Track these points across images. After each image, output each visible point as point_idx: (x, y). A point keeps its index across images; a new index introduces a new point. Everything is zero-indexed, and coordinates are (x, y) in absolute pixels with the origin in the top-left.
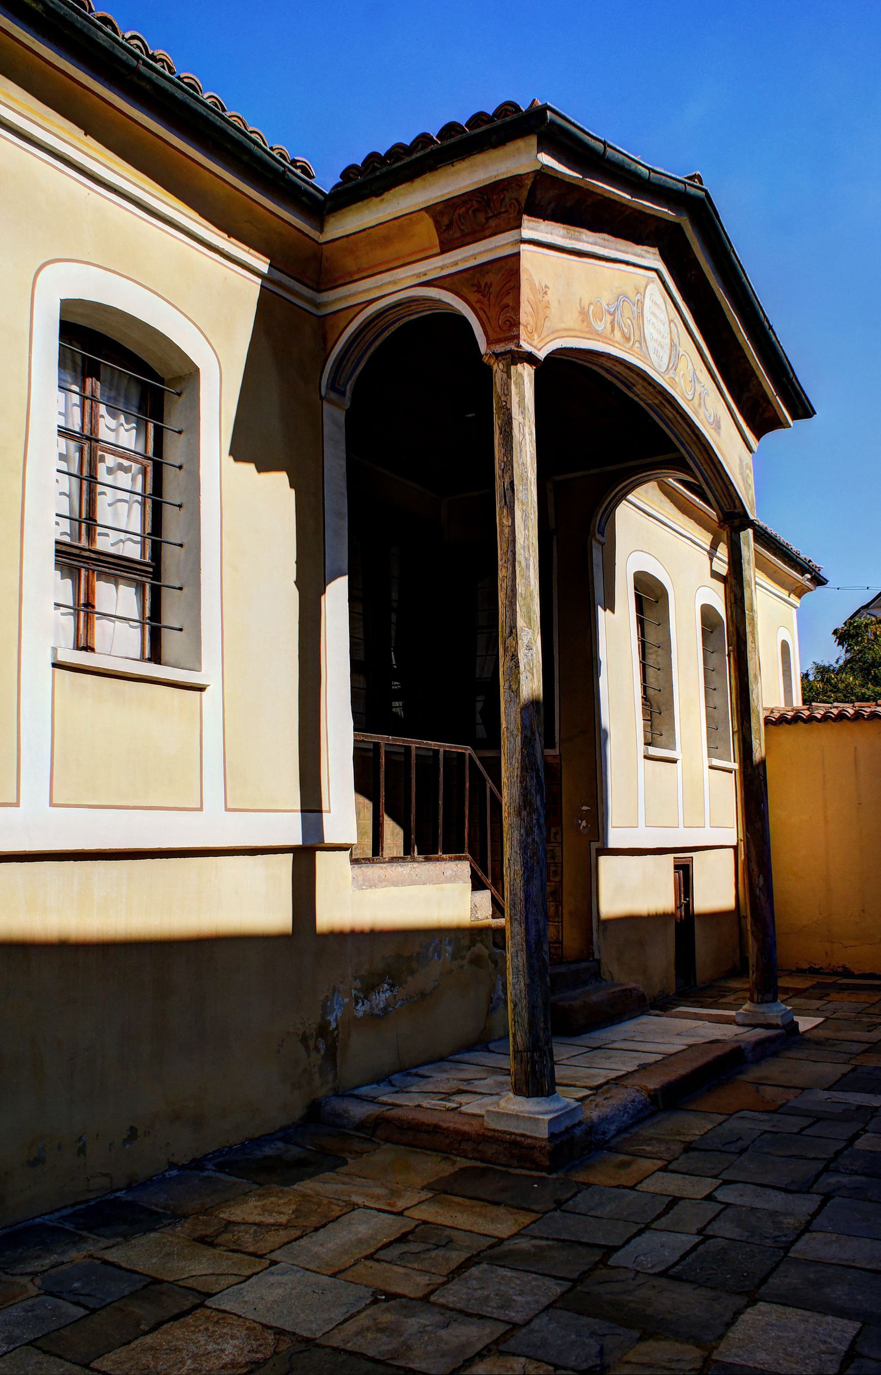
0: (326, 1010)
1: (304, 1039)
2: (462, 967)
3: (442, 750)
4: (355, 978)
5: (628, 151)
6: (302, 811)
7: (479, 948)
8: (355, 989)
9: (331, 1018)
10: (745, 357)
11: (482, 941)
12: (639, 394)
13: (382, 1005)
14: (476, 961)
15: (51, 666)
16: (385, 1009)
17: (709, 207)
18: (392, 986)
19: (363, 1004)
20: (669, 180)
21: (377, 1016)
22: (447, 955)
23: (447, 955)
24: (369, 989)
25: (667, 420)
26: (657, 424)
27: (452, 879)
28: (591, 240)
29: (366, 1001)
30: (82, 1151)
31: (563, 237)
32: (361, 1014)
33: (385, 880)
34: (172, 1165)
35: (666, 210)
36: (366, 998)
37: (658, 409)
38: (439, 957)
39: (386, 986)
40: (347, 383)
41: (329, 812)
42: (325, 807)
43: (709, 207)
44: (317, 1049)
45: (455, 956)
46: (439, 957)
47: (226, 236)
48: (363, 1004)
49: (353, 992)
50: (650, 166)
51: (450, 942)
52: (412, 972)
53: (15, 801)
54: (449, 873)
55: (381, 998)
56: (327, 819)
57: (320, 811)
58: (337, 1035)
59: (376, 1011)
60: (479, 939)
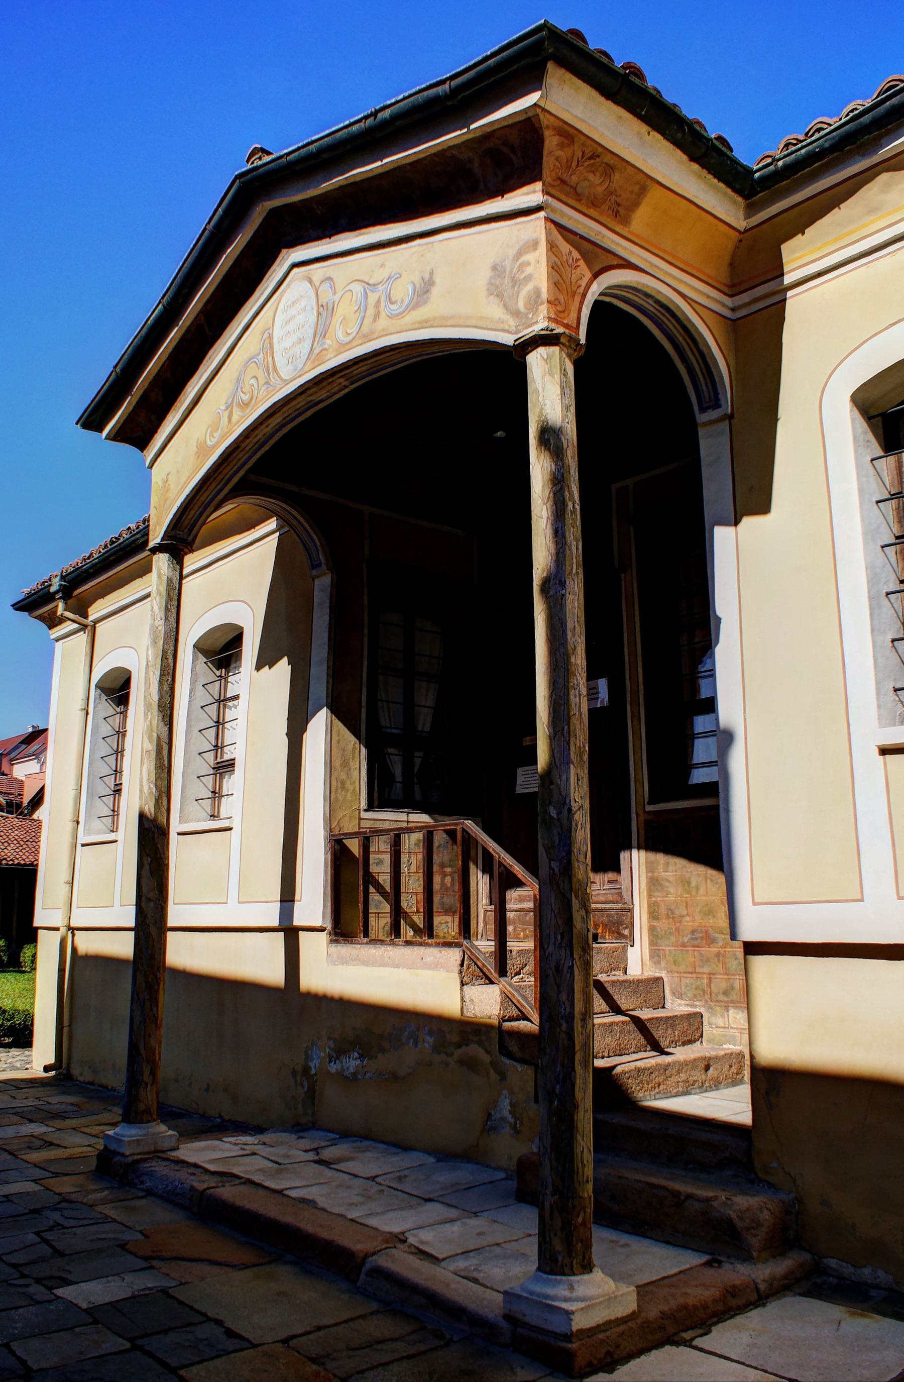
0: (308, 1058)
1: (294, 1073)
2: (447, 1064)
3: (459, 828)
4: (329, 1039)
5: (328, 128)
6: (281, 901)
7: (474, 1050)
8: (329, 1048)
9: (312, 1065)
10: (412, 164)
11: (480, 1043)
12: (325, 396)
13: (352, 1070)
14: (470, 1064)
15: (877, 751)
16: (354, 1074)
17: (249, 176)
18: (369, 1059)
19: (335, 1063)
20: (186, 265)
21: (346, 1077)
22: (427, 1045)
23: (427, 1045)
24: (340, 1052)
25: (375, 369)
26: (259, 459)
27: (435, 966)
28: (198, 378)
29: (337, 1062)
30: (190, 1084)
31: (176, 413)
32: (333, 1071)
33: (356, 960)
34: (220, 1116)
35: (225, 256)
36: (338, 1058)
37: (360, 370)
38: (416, 1044)
39: (356, 1055)
40: (319, 555)
41: (300, 901)
42: (297, 897)
43: (249, 176)
44: (303, 1086)
45: (436, 1049)
46: (416, 1044)
47: (253, 530)
48: (335, 1063)
49: (328, 1050)
50: (157, 302)
51: (430, 1033)
52: (383, 1050)
53: (860, 897)
54: (429, 959)
55: (352, 1063)
56: (298, 907)
57: (293, 901)
58: (317, 1080)
59: (347, 1073)
60: (476, 1039)
